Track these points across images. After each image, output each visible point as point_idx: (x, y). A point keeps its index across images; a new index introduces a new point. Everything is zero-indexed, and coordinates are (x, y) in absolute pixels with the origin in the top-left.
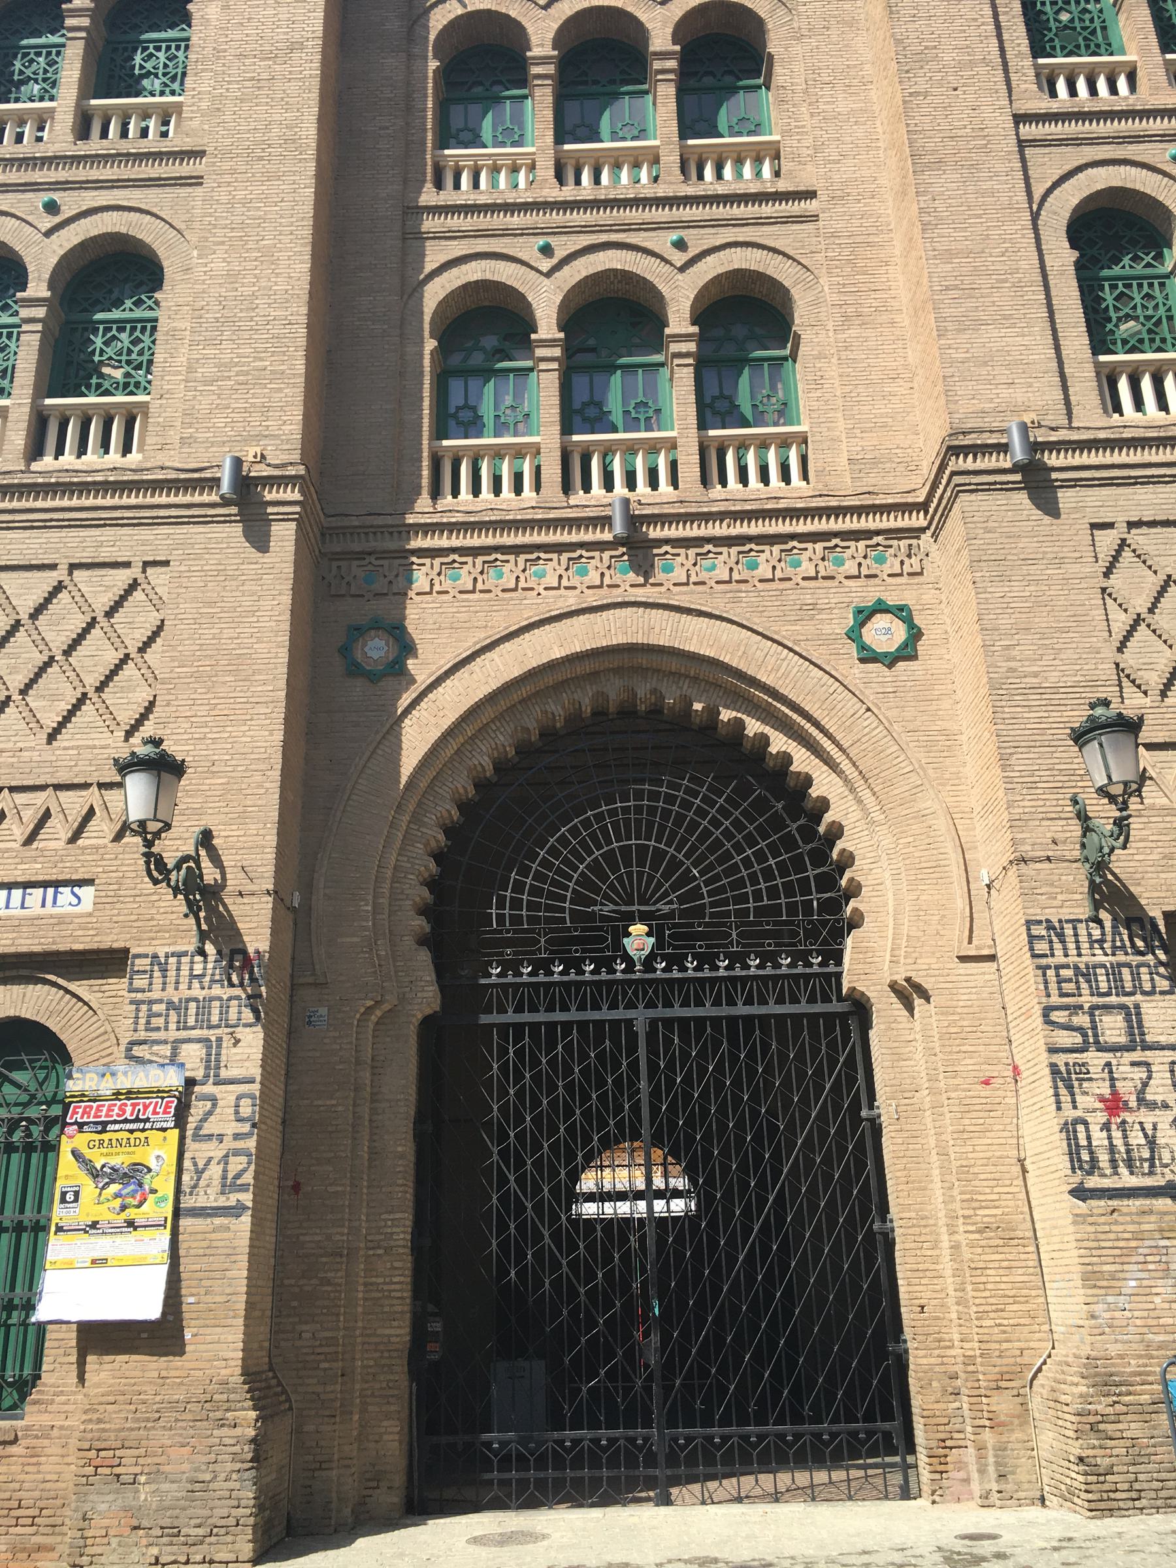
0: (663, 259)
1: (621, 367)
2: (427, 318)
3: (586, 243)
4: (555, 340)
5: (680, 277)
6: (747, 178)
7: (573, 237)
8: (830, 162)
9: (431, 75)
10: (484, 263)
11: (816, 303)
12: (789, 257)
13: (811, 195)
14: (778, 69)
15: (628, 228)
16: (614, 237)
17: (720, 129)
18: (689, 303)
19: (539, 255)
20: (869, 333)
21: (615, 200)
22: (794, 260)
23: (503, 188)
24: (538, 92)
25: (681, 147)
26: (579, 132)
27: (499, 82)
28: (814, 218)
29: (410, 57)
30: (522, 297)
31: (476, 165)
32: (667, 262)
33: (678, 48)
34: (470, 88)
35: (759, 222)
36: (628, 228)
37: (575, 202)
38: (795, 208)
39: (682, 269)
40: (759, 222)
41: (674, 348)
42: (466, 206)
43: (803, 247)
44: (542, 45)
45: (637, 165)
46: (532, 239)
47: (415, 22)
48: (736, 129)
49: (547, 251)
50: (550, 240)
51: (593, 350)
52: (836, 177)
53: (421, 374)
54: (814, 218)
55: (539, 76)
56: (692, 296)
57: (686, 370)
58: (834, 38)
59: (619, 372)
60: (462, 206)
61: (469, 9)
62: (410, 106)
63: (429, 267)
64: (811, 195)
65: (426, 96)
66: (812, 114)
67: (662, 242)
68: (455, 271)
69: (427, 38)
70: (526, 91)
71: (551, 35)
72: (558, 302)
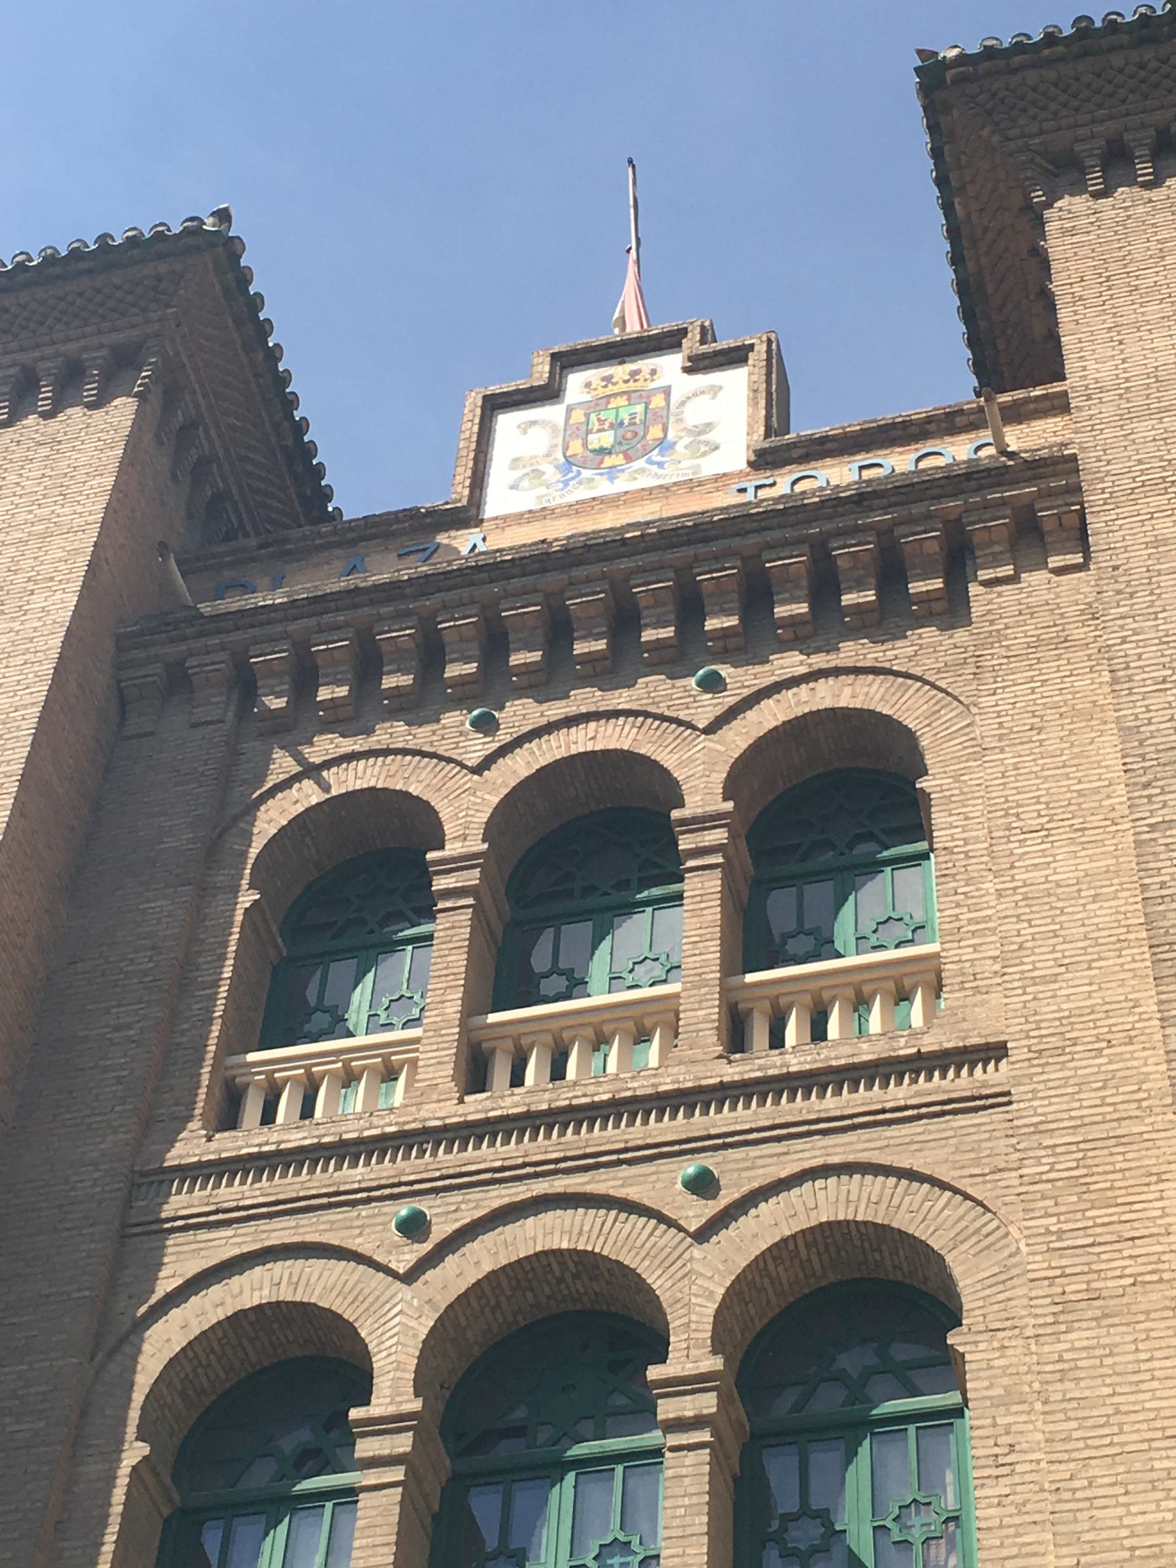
0: (662, 1218)
1: (579, 1464)
2: (138, 1398)
3: (496, 1204)
4: (401, 1417)
5: (697, 1252)
6: (877, 1032)
7: (475, 1194)
8: (1034, 981)
9: (239, 917)
10: (280, 1269)
11: (1003, 1279)
12: (944, 1186)
13: (995, 1052)
14: (938, 818)
15: (592, 1163)
16: (560, 1184)
17: (839, 945)
18: (712, 1307)
19: (396, 1237)
20: (1118, 1335)
21: (571, 1109)
22: (956, 1191)
23: (350, 1112)
24: (692, 886)
25: (724, 991)
26: (792, 946)
27: (869, 837)
28: (1002, 1099)
29: (204, 891)
30: (349, 1330)
31: (309, 1075)
32: (671, 1223)
33: (729, 805)
34: (851, 846)
35: (879, 1119)
36: (592, 1163)
37: (487, 1122)
38: (960, 1083)
39: (702, 1235)
40: (879, 1119)
41: (667, 1409)
42: (260, 1156)
43: (977, 1162)
44: (464, 837)
45: (903, 996)
46: (388, 1207)
47: (225, 830)
48: (873, 941)
49: (414, 1227)
50: (424, 1205)
51: (517, 1432)
52: (1047, 1010)
53: (103, 1522)
54: (1002, 1099)
55: (448, 894)
56: (720, 1291)
57: (691, 1457)
58: (1053, 746)
59: (570, 1477)
60: (251, 1157)
61: (334, 793)
62: (187, 979)
63: (166, 1285)
64: (995, 1052)
65: (223, 958)
66: (1000, 894)
67: (662, 1184)
68: (216, 1291)
69: (244, 855)
70: (923, 846)
71: (484, 817)
72: (423, 1332)
